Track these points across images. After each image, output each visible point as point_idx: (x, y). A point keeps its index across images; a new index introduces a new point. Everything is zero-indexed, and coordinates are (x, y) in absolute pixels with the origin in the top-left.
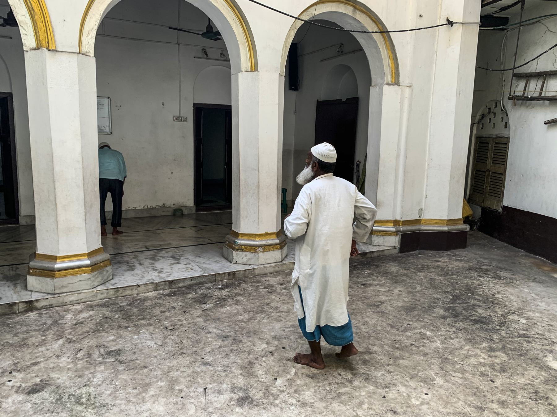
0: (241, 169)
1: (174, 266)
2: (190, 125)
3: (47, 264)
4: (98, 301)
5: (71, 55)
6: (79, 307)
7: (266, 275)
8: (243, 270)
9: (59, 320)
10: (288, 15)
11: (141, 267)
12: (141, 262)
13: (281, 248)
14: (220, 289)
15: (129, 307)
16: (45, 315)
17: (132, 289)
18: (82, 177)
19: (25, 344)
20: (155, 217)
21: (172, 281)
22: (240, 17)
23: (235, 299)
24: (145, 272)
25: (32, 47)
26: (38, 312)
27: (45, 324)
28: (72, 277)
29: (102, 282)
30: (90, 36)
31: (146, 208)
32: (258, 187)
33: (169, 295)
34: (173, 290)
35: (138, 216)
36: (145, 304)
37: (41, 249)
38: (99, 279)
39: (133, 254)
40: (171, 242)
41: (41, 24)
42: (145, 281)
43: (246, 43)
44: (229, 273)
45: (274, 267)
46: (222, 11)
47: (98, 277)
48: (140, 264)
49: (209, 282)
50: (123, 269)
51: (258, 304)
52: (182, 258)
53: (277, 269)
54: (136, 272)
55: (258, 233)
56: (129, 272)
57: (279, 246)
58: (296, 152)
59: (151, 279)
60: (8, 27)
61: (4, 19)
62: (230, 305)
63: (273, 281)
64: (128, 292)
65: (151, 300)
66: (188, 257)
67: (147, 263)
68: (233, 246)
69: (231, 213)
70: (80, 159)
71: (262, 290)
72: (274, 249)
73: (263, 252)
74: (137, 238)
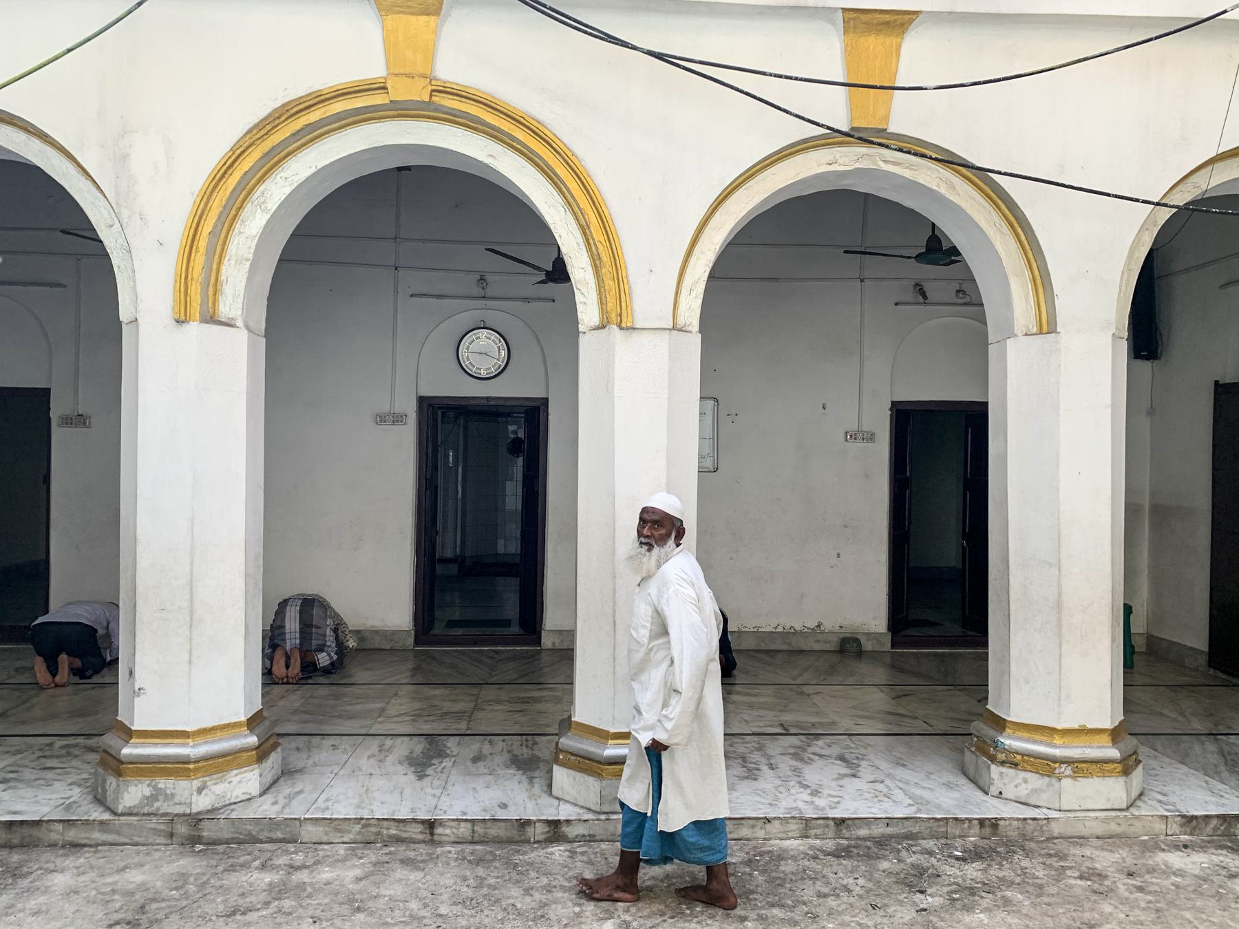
0: (1011, 560)
2: (882, 450)
3: (588, 746)
7: (1082, 840)
8: (1018, 819)
10: (1137, 200)
13: (1126, 772)
14: (958, 858)
15: (748, 870)
16: (581, 858)
17: (753, 827)
19: (543, 916)
21: (843, 820)
22: (1012, 219)
23: (999, 894)
24: (781, 789)
26: (568, 846)
30: (693, 294)
31: (780, 629)
32: (1059, 606)
33: (838, 854)
34: (845, 842)
35: (763, 647)
36: (782, 868)
37: (582, 713)
39: (756, 738)
40: (836, 719)
41: (611, 283)
42: (782, 810)
43: (1027, 273)
44: (982, 822)
45: (1106, 821)
48: (771, 767)
50: (735, 773)
51: (1065, 921)
52: (864, 763)
53: (1113, 828)
55: (1059, 727)
56: (746, 782)
57: (1119, 767)
58: (1156, 509)
59: (796, 808)
60: (550, 284)
61: (548, 273)
62: (987, 910)
63: (1105, 860)
66: (877, 763)
67: (785, 764)
68: (989, 751)
69: (985, 658)
71: (1073, 882)
72: (1104, 774)
73: (1074, 778)
74: (762, 700)
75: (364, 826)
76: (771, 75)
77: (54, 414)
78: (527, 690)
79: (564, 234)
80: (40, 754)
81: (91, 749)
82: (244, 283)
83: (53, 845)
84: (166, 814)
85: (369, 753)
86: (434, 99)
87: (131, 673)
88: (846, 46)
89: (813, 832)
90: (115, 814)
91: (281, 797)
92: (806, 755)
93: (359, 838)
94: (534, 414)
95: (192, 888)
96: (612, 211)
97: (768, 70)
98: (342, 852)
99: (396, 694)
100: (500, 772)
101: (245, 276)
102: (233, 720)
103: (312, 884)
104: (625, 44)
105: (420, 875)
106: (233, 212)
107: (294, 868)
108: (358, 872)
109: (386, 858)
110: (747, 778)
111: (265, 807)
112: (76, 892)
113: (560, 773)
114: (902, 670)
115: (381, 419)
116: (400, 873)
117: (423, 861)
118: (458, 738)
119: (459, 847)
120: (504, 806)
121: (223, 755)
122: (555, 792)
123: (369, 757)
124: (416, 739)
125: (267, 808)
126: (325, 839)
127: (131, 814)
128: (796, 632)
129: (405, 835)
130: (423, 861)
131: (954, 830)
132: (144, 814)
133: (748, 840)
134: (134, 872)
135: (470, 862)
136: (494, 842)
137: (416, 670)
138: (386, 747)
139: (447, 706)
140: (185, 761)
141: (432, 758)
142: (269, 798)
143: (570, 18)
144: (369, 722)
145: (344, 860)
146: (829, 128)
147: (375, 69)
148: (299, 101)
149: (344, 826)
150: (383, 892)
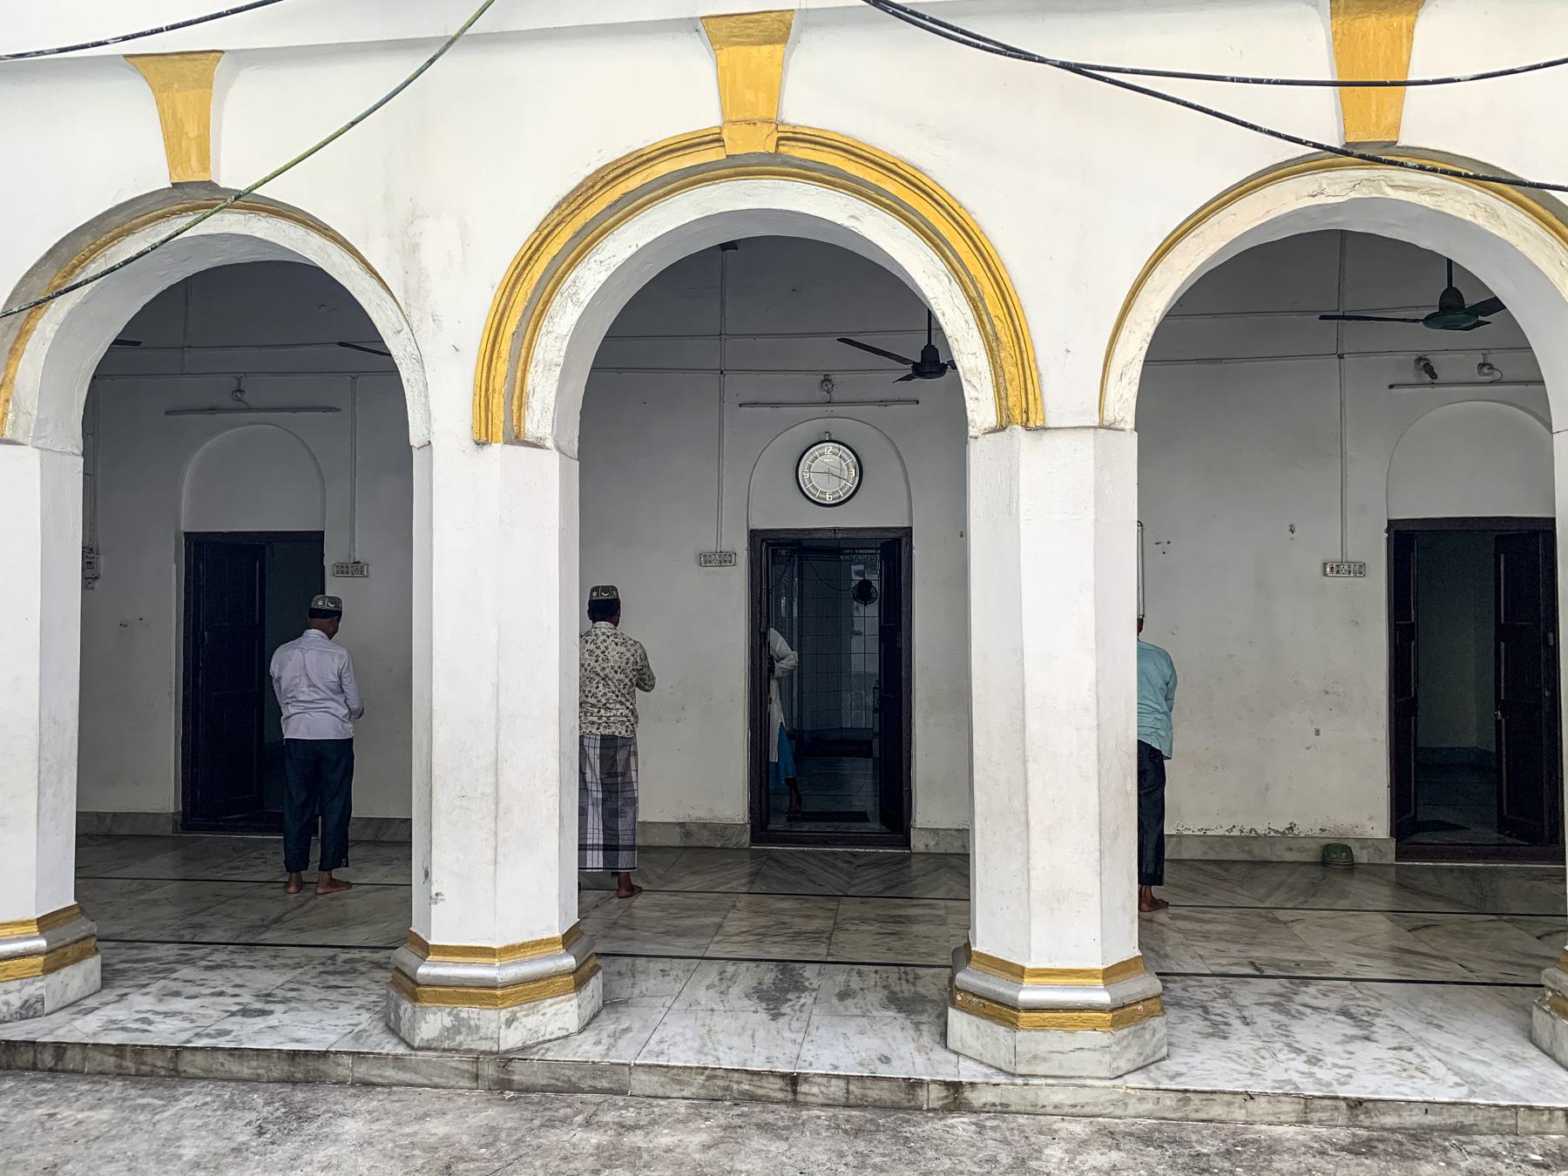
1: (1356, 1046)
4: (1130, 1120)
5: (1078, 433)
6: (1079, 1128)
9: (1030, 1157)
11: (1247, 1030)
12: (1246, 1013)
13: (580, 984)
14: (1537, 1165)
15: (1227, 1165)
16: (991, 1134)
17: (1229, 1104)
18: (1094, 752)
20: (1266, 863)
24: (1264, 1053)
25: (987, 426)
27: (993, 1160)
28: (1060, 1033)
29: (1140, 1062)
30: (1126, 380)
31: (1236, 833)
35: (1212, 856)
36: (1276, 1165)
38: (1132, 1053)
39: (1218, 980)
40: (1330, 957)
41: (1014, 370)
46: (1523, 247)
47: (1129, 1045)
48: (1246, 1021)
49: (1494, 1132)
50: (1194, 1027)
52: (1378, 1021)
54: (1233, 1045)
56: (1212, 1041)
59: (1289, 1082)
61: (916, 366)
64: (1216, 1111)
65: (1292, 1152)
67: (1265, 1018)
70: (1093, 706)
74: (1221, 928)
75: (709, 1078)
76: (1232, 80)
77: (328, 563)
78: (900, 907)
79: (948, 311)
80: (320, 968)
81: (379, 966)
82: (554, 394)
83: (341, 1083)
84: (470, 1051)
85: (707, 982)
86: (782, 149)
87: (427, 874)
88: (1335, 33)
89: (1315, 1116)
90: (412, 1048)
91: (604, 1034)
92: (1294, 1007)
93: (703, 1092)
94: (893, 550)
95: (504, 1147)
96: (1014, 277)
97: (1229, 74)
98: (683, 1110)
99: (734, 906)
100: (875, 1013)
101: (556, 385)
102: (546, 936)
103: (649, 1151)
104: (1029, 57)
105: (783, 1146)
106: (540, 307)
107: (624, 1128)
108: (704, 1137)
109: (738, 1121)
110: (1212, 1035)
111: (586, 1047)
112: (370, 1144)
113: (956, 1019)
114: (1416, 891)
115: (706, 559)
116: (758, 1141)
117: (786, 1128)
118: (817, 966)
119: (830, 1112)
120: (885, 1060)
121: (536, 979)
122: (950, 1045)
123: (708, 988)
124: (764, 965)
125: (588, 1049)
126: (660, 1092)
127: (429, 1049)
128: (1258, 837)
129: (760, 1092)
130: (786, 1128)
131: (1526, 1123)
132: (444, 1050)
133: (1222, 1122)
134: (435, 1121)
135: (846, 1132)
136: (875, 1107)
137: (755, 876)
138: (728, 975)
139: (800, 924)
140: (491, 985)
141: (787, 991)
142: (589, 1036)
143: (956, 30)
144: (704, 941)
145: (685, 1121)
146: (1315, 145)
147: (708, 118)
148: (616, 164)
149: (684, 1077)
150: (739, 1166)
